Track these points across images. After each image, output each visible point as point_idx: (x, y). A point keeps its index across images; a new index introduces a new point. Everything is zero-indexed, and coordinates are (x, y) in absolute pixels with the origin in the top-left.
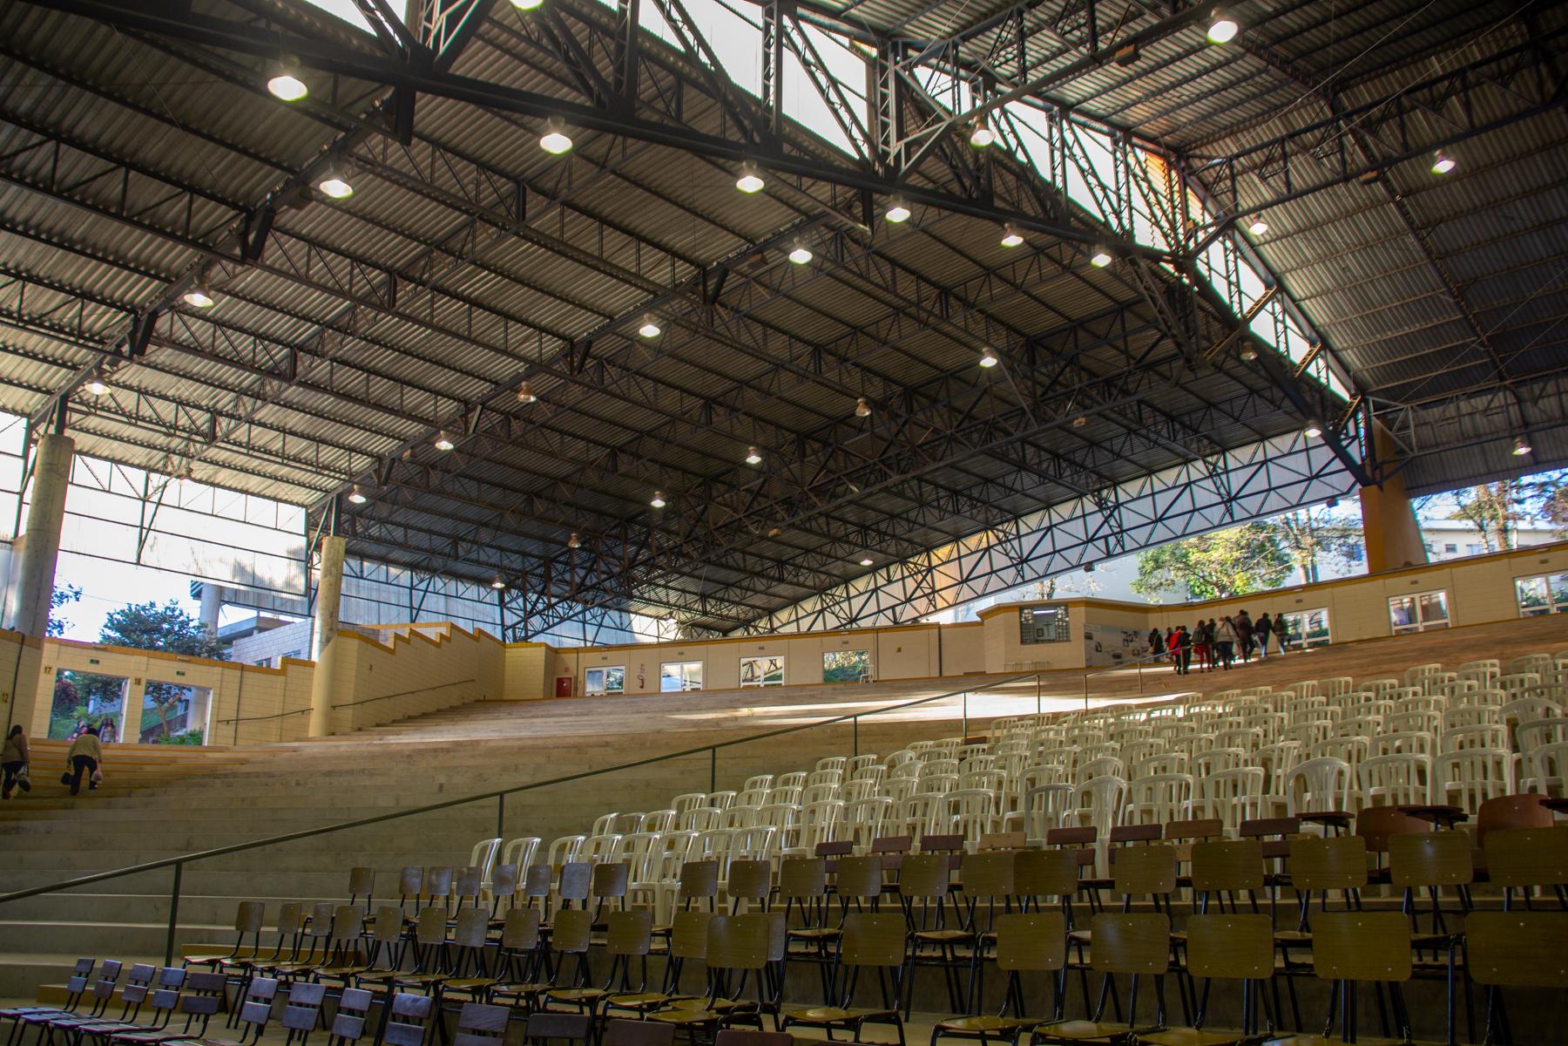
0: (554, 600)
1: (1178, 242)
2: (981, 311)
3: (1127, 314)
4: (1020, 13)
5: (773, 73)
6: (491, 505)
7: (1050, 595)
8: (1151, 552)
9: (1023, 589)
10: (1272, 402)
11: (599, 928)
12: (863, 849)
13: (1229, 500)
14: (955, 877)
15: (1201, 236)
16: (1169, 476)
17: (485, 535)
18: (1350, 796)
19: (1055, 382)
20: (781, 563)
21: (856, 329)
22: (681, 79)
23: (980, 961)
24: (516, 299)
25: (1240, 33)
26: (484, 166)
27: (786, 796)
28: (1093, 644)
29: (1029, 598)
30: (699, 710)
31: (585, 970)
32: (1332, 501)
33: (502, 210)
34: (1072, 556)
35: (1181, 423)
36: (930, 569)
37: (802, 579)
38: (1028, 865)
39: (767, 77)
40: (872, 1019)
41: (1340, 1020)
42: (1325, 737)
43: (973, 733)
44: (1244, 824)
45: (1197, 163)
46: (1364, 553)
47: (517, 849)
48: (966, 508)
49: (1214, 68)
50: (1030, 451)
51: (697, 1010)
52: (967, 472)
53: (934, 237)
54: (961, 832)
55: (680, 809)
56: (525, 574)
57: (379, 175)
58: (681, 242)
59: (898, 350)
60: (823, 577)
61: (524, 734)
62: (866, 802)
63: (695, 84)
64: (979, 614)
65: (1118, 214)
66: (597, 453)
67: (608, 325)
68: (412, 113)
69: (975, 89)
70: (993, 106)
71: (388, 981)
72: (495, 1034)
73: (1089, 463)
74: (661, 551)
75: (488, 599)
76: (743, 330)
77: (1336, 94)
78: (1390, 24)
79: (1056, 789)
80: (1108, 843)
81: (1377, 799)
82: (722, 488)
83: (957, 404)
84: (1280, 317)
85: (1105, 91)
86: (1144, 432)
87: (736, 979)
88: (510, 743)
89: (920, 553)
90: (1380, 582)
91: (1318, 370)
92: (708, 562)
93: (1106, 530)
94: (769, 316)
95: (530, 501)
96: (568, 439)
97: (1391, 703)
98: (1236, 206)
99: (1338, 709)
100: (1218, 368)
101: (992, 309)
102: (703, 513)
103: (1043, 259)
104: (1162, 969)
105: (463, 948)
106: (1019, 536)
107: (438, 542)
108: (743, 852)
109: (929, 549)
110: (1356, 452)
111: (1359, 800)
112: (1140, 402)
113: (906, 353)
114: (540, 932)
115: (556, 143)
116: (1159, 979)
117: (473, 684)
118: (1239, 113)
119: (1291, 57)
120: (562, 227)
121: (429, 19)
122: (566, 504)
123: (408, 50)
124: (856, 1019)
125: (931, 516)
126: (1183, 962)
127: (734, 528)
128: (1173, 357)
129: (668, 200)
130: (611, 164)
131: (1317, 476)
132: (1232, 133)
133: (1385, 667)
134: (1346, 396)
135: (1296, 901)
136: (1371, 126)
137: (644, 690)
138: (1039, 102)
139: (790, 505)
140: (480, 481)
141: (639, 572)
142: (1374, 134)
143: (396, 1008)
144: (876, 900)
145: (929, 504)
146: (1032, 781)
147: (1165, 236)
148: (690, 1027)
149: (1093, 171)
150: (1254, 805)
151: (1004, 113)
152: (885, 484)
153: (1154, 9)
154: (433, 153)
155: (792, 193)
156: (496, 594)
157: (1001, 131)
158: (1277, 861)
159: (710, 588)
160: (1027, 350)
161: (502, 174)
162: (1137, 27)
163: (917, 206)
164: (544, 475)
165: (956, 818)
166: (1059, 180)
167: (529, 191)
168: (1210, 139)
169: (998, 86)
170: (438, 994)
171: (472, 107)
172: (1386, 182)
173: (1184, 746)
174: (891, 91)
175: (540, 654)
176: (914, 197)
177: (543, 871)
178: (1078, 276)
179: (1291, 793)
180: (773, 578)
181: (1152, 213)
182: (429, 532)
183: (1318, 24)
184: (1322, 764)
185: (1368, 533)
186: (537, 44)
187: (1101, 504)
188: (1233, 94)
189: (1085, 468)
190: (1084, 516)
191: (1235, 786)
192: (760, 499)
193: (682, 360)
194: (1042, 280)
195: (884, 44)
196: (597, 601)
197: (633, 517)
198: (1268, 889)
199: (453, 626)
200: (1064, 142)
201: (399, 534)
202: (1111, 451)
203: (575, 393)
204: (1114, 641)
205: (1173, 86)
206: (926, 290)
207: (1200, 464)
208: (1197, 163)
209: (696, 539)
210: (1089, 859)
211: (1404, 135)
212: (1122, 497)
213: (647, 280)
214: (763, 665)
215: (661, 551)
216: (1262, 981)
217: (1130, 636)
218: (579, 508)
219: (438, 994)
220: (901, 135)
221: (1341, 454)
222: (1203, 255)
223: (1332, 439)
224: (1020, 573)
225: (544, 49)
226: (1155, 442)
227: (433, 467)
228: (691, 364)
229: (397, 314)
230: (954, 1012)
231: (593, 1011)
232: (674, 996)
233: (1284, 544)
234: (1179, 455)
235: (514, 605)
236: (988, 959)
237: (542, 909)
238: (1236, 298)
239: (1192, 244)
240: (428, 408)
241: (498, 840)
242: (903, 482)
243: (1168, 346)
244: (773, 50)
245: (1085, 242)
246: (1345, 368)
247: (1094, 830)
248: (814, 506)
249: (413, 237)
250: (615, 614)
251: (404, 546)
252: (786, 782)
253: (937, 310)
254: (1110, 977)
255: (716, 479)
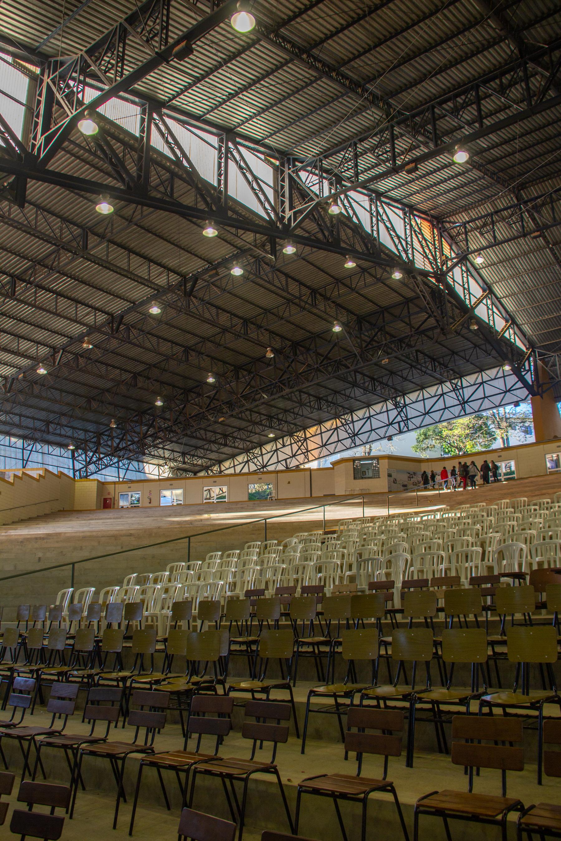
0: (102, 456)
1: (437, 266)
2: (333, 302)
3: (410, 304)
4: (355, 144)
5: (223, 173)
6: (68, 404)
7: (369, 453)
8: (422, 430)
9: (355, 450)
10: (486, 351)
11: (127, 638)
12: (270, 593)
13: (463, 403)
14: (319, 608)
15: (449, 263)
16: (432, 390)
17: (64, 421)
18: (526, 562)
19: (372, 340)
20: (225, 436)
21: (266, 311)
22: (173, 175)
23: (333, 654)
24: (82, 292)
25: (470, 158)
26: (65, 220)
27: (228, 564)
28: (392, 479)
29: (358, 455)
30: (181, 515)
31: (120, 661)
32: (517, 404)
33: (74, 244)
34: (381, 432)
35: (438, 362)
36: (306, 439)
37: (237, 444)
38: (358, 601)
39: (220, 175)
40: (276, 687)
41: (521, 681)
42: (513, 531)
43: (329, 528)
44: (472, 578)
45: (447, 225)
46: (533, 431)
47: (82, 594)
48: (325, 407)
49: (457, 176)
50: (359, 377)
51: (181, 683)
52: (326, 388)
53: (308, 262)
54: (322, 584)
55: (171, 571)
56: (86, 441)
57: (6, 223)
58: (172, 263)
59: (289, 322)
60: (248, 443)
61: (85, 529)
62: (272, 567)
63: (181, 178)
64: (331, 464)
65: (406, 252)
66: (126, 376)
67: (132, 307)
68: (25, 190)
69: (331, 184)
70: (341, 193)
71: (11, 669)
72: (70, 699)
73: (390, 383)
74: (160, 429)
75: (66, 455)
76: (206, 311)
77: (519, 191)
78: (546, 156)
79: (373, 560)
80: (400, 588)
81: (540, 564)
82: (194, 395)
83: (321, 351)
84: (490, 307)
85: (400, 186)
86: (419, 367)
87: (202, 666)
88: (78, 534)
89: (300, 431)
90: (541, 446)
91: (510, 334)
92: (186, 435)
93: (399, 419)
94: (219, 303)
95: (89, 402)
96: (110, 368)
97: (547, 512)
98: (468, 248)
99: (520, 515)
100: (458, 333)
101: (339, 301)
102: (183, 409)
103: (367, 275)
104: (429, 658)
105: (52, 650)
106: (353, 422)
107: (38, 424)
108: (206, 594)
109: (305, 428)
110: (529, 378)
111: (531, 564)
112: (417, 351)
113: (293, 324)
114: (95, 641)
115: (105, 208)
116: (427, 663)
117: (57, 502)
118: (469, 200)
119: (496, 171)
120: (108, 253)
121: (35, 138)
122: (109, 404)
123: (23, 155)
124: (267, 687)
125: (306, 411)
126: (440, 653)
127: (200, 417)
128: (435, 327)
129: (166, 240)
130: (135, 220)
131: (509, 391)
132: (466, 210)
133: (544, 491)
134: (524, 349)
135: (498, 618)
136: (537, 208)
137: (151, 505)
138: (365, 192)
139: (230, 404)
140: (61, 391)
141: (149, 440)
142: (539, 212)
143: (15, 685)
144: (277, 621)
145: (305, 405)
146: (360, 555)
147: (431, 263)
148: (178, 693)
149: (393, 228)
150: (477, 567)
151: (346, 197)
152: (281, 394)
153: (426, 144)
154: (37, 212)
155: (232, 238)
156: (70, 452)
157: (344, 206)
158: (489, 598)
159: (187, 449)
160: (358, 322)
161: (75, 224)
162: (417, 153)
163: (299, 246)
164: (96, 388)
165: (320, 575)
166: (375, 233)
167: (89, 234)
168: (454, 213)
169: (343, 183)
170: (38, 676)
171: (58, 187)
172: (545, 238)
173: (440, 535)
174: (286, 184)
175: (94, 485)
176: (298, 240)
177: (96, 607)
178: (385, 284)
179: (495, 561)
180: (221, 444)
181: (425, 252)
182: (33, 418)
183: (509, 155)
184: (511, 546)
185: (535, 420)
186: (95, 154)
187: (396, 405)
188: (466, 190)
189: (388, 386)
190: (387, 411)
191: (467, 557)
192: (214, 401)
193: (173, 326)
194: (366, 286)
195: (282, 159)
196: (126, 456)
197: (145, 412)
198: (484, 613)
199: (46, 470)
200: (378, 212)
201: (16, 419)
202: (402, 377)
203: (114, 344)
204: (403, 478)
205: (435, 185)
206: (304, 290)
207: (448, 384)
208: (447, 225)
209: (180, 423)
210: (390, 597)
211: (553, 214)
212: (408, 401)
213: (154, 283)
214: (216, 491)
215: (160, 429)
216: (481, 664)
217: (411, 475)
218: (116, 406)
219: (38, 676)
220: (291, 208)
221: (522, 379)
222: (450, 274)
223: (517, 372)
224: (353, 441)
225: (99, 157)
226: (425, 372)
227: (36, 383)
228: (177, 328)
229: (16, 299)
230: (319, 680)
231: (124, 684)
232: (169, 675)
233: (492, 426)
234: (437, 379)
235: (80, 458)
236: (337, 652)
237: (96, 627)
238: (467, 297)
239: (444, 268)
240: (33, 351)
241: (71, 589)
242: (291, 393)
243: (432, 322)
244: (223, 160)
245: (388, 266)
246: (524, 335)
247: (393, 582)
248: (243, 405)
249: (24, 257)
250: (135, 463)
251: (19, 426)
252: (229, 556)
253: (310, 301)
254: (402, 663)
255: (190, 391)
